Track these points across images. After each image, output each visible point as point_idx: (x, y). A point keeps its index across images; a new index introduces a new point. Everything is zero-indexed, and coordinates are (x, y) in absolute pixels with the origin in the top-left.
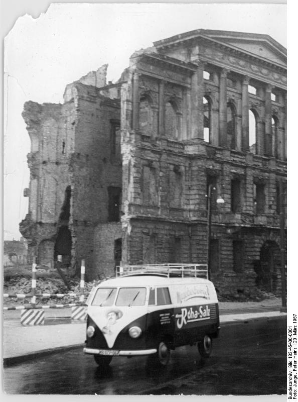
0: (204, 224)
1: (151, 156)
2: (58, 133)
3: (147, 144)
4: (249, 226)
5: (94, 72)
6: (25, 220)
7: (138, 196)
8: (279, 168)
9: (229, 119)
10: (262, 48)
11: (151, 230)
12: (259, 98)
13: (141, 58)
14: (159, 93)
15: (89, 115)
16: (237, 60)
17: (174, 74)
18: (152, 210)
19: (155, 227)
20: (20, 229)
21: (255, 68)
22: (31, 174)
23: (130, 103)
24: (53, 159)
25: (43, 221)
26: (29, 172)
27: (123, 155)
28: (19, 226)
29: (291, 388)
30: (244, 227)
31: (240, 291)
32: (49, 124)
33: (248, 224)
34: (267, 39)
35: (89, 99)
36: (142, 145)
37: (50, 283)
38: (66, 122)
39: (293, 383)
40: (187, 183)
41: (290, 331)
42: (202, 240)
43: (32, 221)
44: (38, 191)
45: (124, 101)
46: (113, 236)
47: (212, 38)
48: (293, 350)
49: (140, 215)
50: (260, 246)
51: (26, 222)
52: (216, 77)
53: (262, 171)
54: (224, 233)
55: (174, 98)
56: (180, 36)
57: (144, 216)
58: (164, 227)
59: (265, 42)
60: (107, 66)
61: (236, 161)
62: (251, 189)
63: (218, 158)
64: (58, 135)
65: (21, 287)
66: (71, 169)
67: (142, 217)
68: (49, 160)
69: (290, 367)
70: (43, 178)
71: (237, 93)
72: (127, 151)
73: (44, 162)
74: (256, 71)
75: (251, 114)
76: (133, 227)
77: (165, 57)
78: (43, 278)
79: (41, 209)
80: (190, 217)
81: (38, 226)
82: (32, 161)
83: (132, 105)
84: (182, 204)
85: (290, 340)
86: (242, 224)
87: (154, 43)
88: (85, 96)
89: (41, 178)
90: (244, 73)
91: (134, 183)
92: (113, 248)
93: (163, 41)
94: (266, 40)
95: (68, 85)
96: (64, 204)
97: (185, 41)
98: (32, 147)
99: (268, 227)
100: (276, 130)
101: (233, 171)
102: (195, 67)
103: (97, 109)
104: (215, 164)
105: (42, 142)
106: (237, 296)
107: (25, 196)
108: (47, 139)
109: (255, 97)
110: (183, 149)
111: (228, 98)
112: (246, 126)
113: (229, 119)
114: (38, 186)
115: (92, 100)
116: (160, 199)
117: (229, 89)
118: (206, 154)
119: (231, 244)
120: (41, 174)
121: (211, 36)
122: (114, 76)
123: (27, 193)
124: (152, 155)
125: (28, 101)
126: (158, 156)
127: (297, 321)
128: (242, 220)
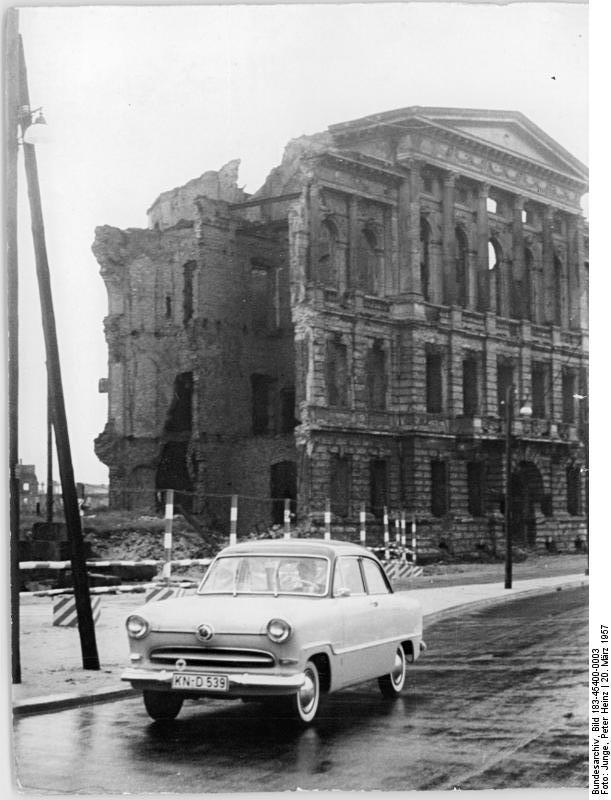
2: (157, 281)
3: (332, 305)
4: (494, 438)
5: (215, 174)
6: (104, 433)
10: (508, 133)
12: (503, 220)
13: (322, 159)
14: (348, 217)
15: (218, 251)
19: (348, 444)
21: (497, 168)
22: (110, 353)
23: (305, 236)
24: (150, 327)
25: (136, 435)
26: (107, 350)
27: (295, 324)
28: (93, 444)
29: (596, 772)
30: (487, 441)
31: (480, 547)
33: (492, 435)
36: (326, 307)
37: (182, 539)
38: (171, 262)
39: (601, 763)
40: (395, 368)
41: (595, 658)
42: (422, 463)
43: (116, 434)
44: (124, 382)
45: (296, 233)
46: (267, 460)
47: (435, 121)
48: (600, 696)
49: (325, 423)
51: (106, 436)
52: (436, 186)
53: (509, 344)
54: (453, 451)
56: (379, 117)
57: (332, 425)
60: (237, 162)
61: (470, 329)
63: (444, 325)
65: (131, 548)
66: (194, 346)
68: (143, 329)
69: (596, 729)
70: (132, 361)
72: (305, 322)
73: (134, 333)
74: (499, 174)
76: (316, 444)
77: (361, 157)
79: (131, 414)
80: (400, 424)
81: (128, 443)
83: (309, 239)
84: (388, 402)
85: (595, 676)
86: (484, 434)
88: (213, 219)
89: (129, 360)
91: (315, 371)
93: (347, 125)
94: (516, 122)
96: (172, 405)
98: (110, 306)
99: (525, 439)
101: (466, 346)
102: (406, 170)
103: (232, 241)
104: (438, 336)
105: (129, 297)
106: (476, 554)
107: (101, 391)
108: (139, 292)
110: (388, 311)
114: (124, 375)
115: (224, 226)
117: (456, 205)
118: (425, 319)
119: (463, 469)
120: (129, 352)
121: (431, 117)
122: (252, 183)
123: (104, 386)
124: (341, 323)
126: (349, 324)
127: (609, 639)
128: (483, 428)
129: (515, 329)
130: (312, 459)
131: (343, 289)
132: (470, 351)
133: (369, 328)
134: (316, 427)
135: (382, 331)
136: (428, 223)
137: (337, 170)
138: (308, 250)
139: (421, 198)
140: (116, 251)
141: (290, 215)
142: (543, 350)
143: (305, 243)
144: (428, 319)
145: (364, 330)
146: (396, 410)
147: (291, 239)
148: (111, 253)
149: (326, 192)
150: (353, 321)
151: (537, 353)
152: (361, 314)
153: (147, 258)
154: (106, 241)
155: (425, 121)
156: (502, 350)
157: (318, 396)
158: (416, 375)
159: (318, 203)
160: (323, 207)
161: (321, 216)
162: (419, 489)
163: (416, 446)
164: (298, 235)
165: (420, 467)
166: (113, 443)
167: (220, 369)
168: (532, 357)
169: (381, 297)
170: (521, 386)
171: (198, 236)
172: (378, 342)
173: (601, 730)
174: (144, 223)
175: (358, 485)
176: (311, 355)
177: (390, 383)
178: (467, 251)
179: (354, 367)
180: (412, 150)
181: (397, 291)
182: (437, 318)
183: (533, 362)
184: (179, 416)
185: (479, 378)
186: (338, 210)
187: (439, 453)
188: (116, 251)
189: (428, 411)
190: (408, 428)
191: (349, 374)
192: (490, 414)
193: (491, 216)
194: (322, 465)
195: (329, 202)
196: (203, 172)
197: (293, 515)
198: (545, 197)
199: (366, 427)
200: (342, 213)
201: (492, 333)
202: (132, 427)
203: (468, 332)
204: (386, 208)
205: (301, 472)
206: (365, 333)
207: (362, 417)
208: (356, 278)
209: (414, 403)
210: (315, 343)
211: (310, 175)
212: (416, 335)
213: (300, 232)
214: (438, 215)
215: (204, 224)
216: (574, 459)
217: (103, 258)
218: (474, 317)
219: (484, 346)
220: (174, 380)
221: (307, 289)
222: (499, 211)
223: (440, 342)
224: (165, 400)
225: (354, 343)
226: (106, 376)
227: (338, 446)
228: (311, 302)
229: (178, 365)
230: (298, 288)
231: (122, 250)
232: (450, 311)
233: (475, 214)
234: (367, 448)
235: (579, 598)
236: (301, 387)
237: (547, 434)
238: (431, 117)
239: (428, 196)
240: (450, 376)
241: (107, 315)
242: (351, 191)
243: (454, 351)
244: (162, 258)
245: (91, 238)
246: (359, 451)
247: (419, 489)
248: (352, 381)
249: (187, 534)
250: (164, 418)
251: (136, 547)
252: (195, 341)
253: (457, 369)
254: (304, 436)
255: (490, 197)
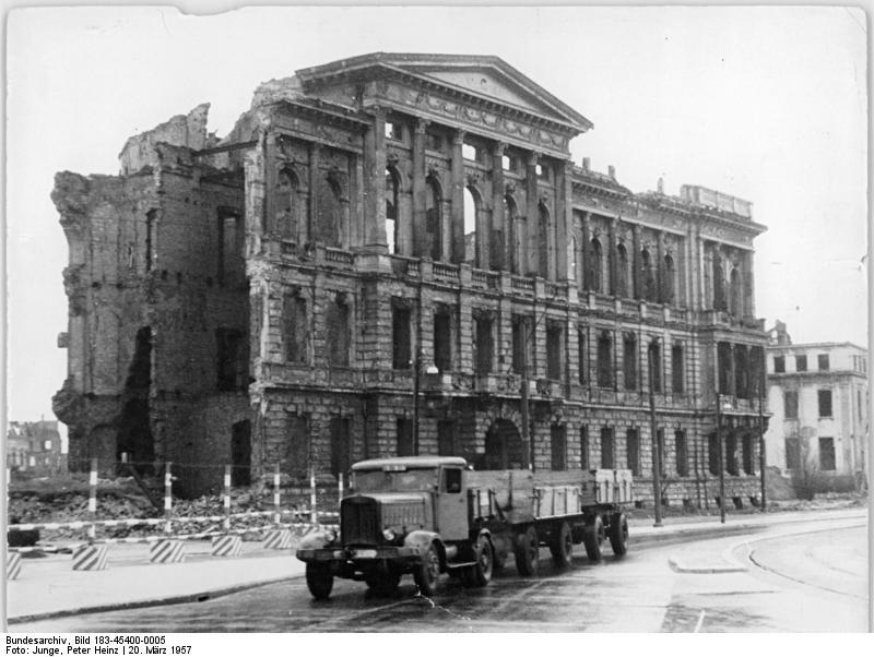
0: (387, 394)
1: (296, 278)
2: (120, 230)
3: (290, 257)
4: (466, 395)
5: (184, 118)
6: (62, 391)
7: (277, 349)
8: (516, 291)
9: (430, 205)
10: (485, 77)
11: (300, 407)
12: (480, 166)
16: (441, 101)
17: (334, 131)
18: (301, 372)
20: (54, 408)
22: (70, 306)
24: (112, 279)
25: (96, 392)
26: (67, 303)
32: (102, 214)
33: (464, 392)
34: (495, 63)
35: (179, 172)
36: (283, 259)
37: (127, 502)
38: (135, 210)
43: (75, 392)
44: (84, 337)
47: (400, 67)
49: (281, 381)
50: (486, 428)
51: (65, 394)
52: (406, 133)
53: (487, 297)
55: (335, 174)
56: (344, 64)
57: (288, 382)
58: (321, 400)
59: (491, 68)
60: (207, 106)
62: (468, 328)
64: (119, 235)
65: (75, 512)
66: (152, 299)
67: (284, 385)
70: (93, 314)
71: (442, 159)
72: (259, 272)
73: (96, 285)
75: (467, 194)
76: (271, 402)
78: (113, 495)
81: (87, 400)
82: (73, 283)
83: (265, 189)
84: (351, 359)
87: (297, 72)
88: (174, 166)
90: (455, 124)
91: (271, 326)
92: (230, 439)
93: (313, 71)
95: (132, 138)
96: (134, 361)
97: (353, 72)
99: (499, 396)
100: (511, 220)
101: (437, 299)
102: (372, 117)
103: (194, 190)
104: (406, 289)
105: (91, 247)
107: (60, 346)
108: (100, 242)
109: (474, 165)
110: (352, 262)
111: (427, 169)
112: (459, 218)
113: (430, 205)
114: (85, 328)
115: (185, 174)
116: (313, 353)
117: (427, 152)
118: (391, 272)
119: (434, 428)
120: (89, 307)
121: (397, 63)
122: (222, 126)
123: (64, 341)
124: (300, 276)
125: (62, 170)
126: (309, 277)
128: (454, 385)
129: (493, 281)
130: (266, 419)
131: (303, 240)
132: (442, 305)
133: (329, 281)
134: (269, 384)
135: (345, 284)
136: (397, 171)
137: (296, 117)
138: (265, 200)
139: (388, 146)
140: (77, 198)
141: (246, 164)
142: (525, 303)
143: (262, 194)
144: (395, 272)
145: (325, 283)
146: (360, 366)
147: (246, 188)
148: (72, 201)
149: (285, 141)
150: (313, 273)
151: (517, 306)
152: (321, 266)
153: (109, 206)
154: (66, 189)
155: (390, 67)
156: (478, 303)
157: (273, 352)
158: (382, 331)
159: (275, 151)
160: (282, 156)
161: (280, 165)
162: (382, 449)
163: (380, 403)
164: (253, 185)
165: (385, 426)
166: (70, 402)
167: (180, 324)
168: (512, 310)
169: (346, 248)
170: (500, 341)
171: (158, 184)
172: (341, 295)
173: (77, 646)
174: (113, 168)
175: (317, 445)
176: (266, 309)
177: (353, 337)
178: (441, 200)
179: (313, 322)
180: (377, 96)
181: (362, 241)
182: (406, 270)
183: (513, 314)
184: (139, 373)
185: (453, 333)
186: (298, 159)
187: (405, 411)
188: (77, 198)
189: (395, 366)
190: (372, 385)
191: (309, 329)
192: (463, 370)
193: (468, 163)
194: (278, 424)
195: (289, 150)
196: (171, 116)
197: (175, 478)
198: (529, 142)
199: (326, 384)
200: (301, 161)
201: (466, 285)
202: (92, 383)
203: (439, 285)
204: (351, 156)
205: (256, 432)
206: (326, 287)
207: (323, 374)
208: (316, 229)
209: (378, 359)
210: (271, 297)
211: (267, 122)
212: (382, 288)
213: (256, 181)
214: (408, 163)
215: (163, 172)
216: (558, 417)
217: (63, 206)
218: (449, 269)
219: (458, 300)
220: (135, 333)
221: (263, 241)
222: (479, 158)
223: (408, 296)
224: (127, 356)
225: (314, 297)
226: (65, 330)
227: (296, 405)
228: (267, 255)
229: (140, 318)
230: (253, 240)
231: (84, 198)
232: (419, 263)
233: (450, 162)
234: (328, 406)
235: (388, 560)
236: (255, 344)
237: (523, 391)
238: (397, 63)
239: (399, 144)
240: (420, 331)
241: (67, 266)
242: (311, 139)
243: (423, 305)
244: (125, 206)
245: (51, 186)
246: (319, 410)
247: (382, 449)
248: (312, 336)
249: (134, 497)
250: (126, 375)
251: (80, 510)
252: (152, 294)
253: (426, 323)
254: (258, 395)
255: (465, 142)
